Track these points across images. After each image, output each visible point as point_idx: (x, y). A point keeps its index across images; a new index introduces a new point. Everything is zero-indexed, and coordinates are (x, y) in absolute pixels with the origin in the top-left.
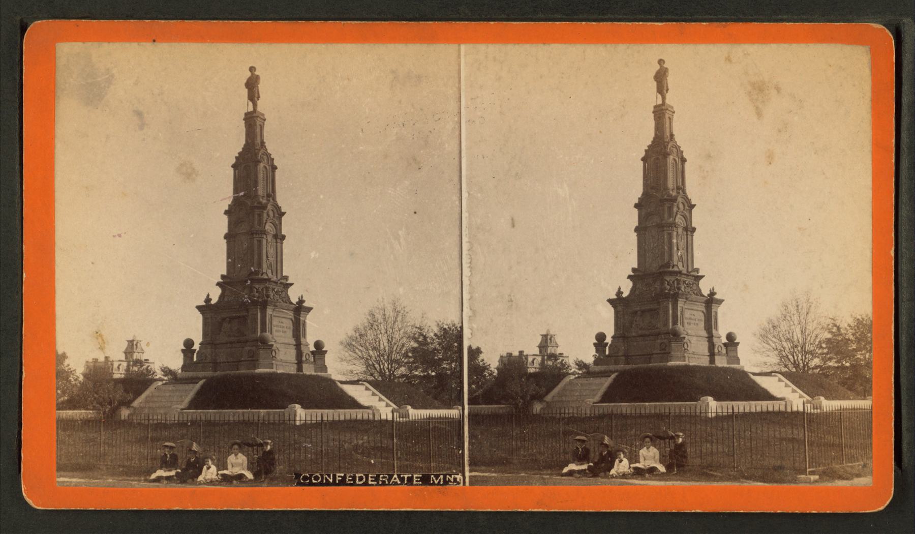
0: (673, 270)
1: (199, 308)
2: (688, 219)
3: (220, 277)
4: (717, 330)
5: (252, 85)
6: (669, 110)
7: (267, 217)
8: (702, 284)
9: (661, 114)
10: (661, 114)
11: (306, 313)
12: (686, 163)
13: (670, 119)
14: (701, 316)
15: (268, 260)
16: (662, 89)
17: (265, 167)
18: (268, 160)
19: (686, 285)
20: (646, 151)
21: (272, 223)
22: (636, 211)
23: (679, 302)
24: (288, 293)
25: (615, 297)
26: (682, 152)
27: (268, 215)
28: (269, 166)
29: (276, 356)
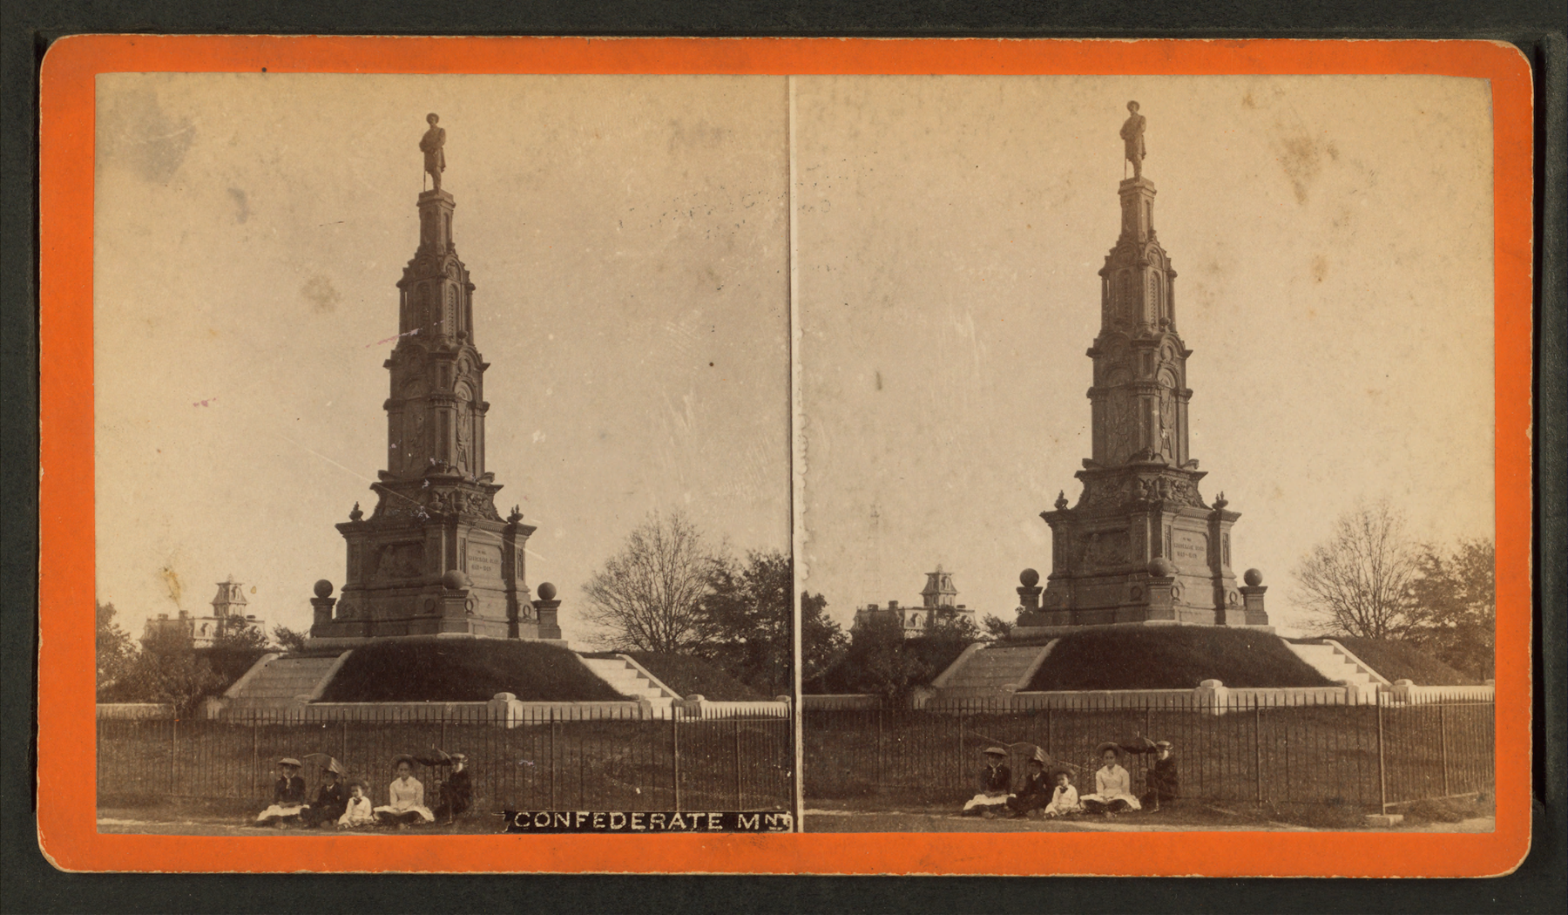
0: (449, 474)
1: (1046, 516)
2: (1179, 375)
4: (1228, 565)
5: (432, 145)
6: (446, 202)
7: (1161, 359)
8: (1203, 486)
9: (1132, 194)
10: (1132, 194)
11: (525, 537)
12: (1175, 279)
13: (1148, 203)
14: (1202, 542)
15: (460, 445)
16: (1134, 152)
17: (454, 286)
18: (459, 274)
19: (1175, 489)
20: (1107, 258)
21: (467, 383)
22: (1090, 362)
25: (1055, 509)
28: (1163, 271)
29: (473, 611)
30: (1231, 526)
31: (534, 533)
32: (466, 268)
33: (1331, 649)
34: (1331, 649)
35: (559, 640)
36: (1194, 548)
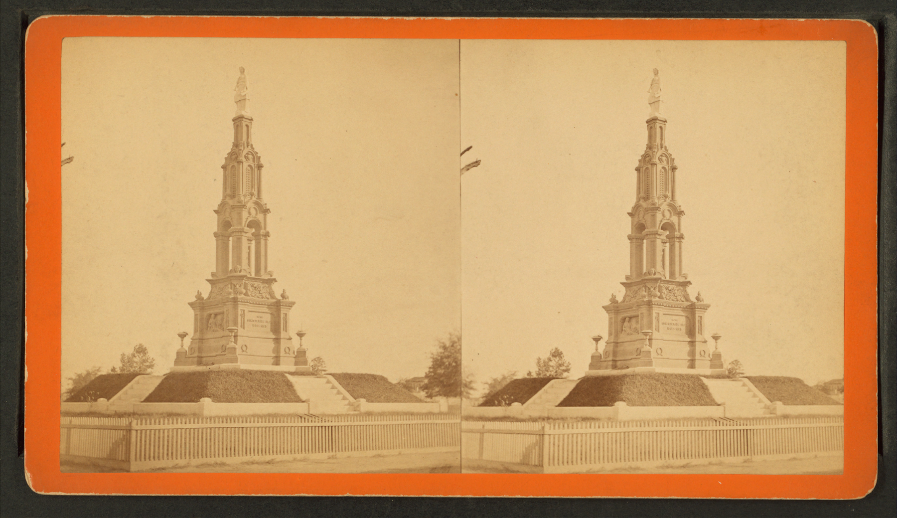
1: (191, 304)
3: (624, 277)
4: (701, 332)
7: (248, 216)
8: (689, 289)
17: (664, 168)
18: (254, 159)
23: (282, 309)
24: (625, 292)
26: (259, 158)
27: (664, 216)
30: (290, 309)
31: (709, 309)
32: (673, 157)
33: (741, 383)
34: (741, 383)
35: (651, 367)
36: (679, 325)
